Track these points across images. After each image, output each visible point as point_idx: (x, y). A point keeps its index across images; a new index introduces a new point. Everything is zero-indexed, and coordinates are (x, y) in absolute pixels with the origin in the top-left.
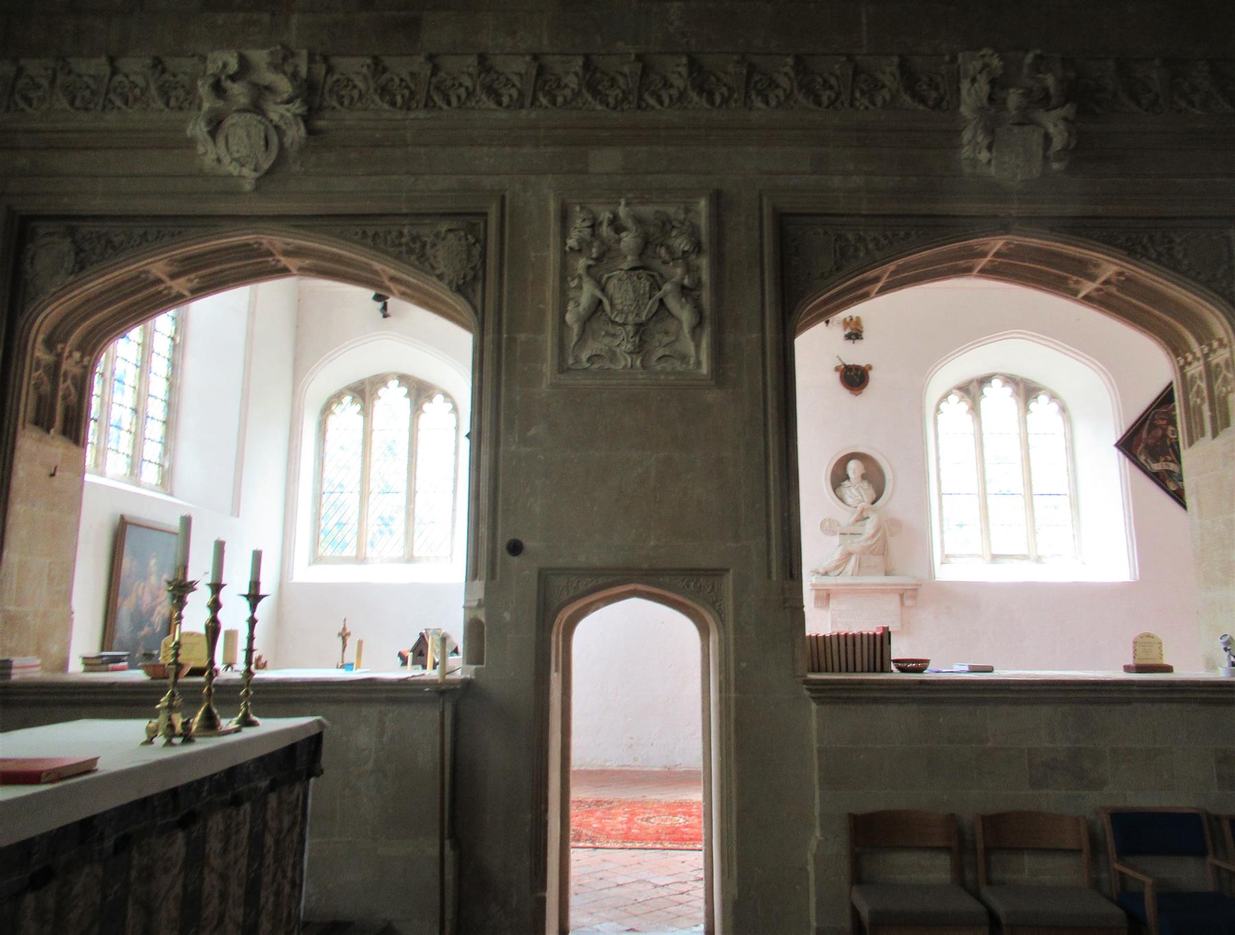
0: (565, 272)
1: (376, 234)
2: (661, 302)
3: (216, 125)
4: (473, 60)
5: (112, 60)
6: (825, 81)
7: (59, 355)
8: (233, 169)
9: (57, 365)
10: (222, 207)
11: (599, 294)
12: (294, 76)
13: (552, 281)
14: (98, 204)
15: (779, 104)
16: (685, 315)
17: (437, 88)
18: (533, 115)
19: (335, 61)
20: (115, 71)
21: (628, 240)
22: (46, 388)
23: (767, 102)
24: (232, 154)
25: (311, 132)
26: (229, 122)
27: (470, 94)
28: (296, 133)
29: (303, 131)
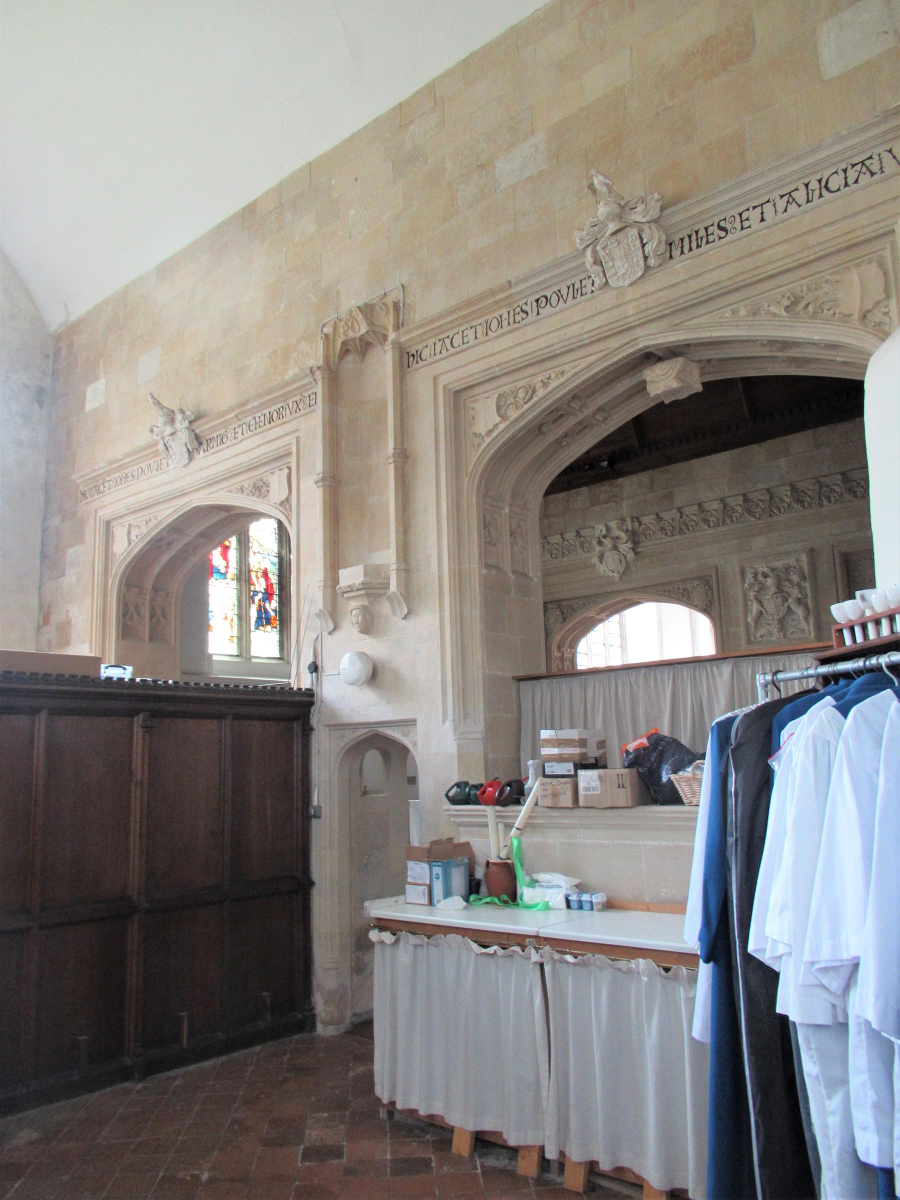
0: (746, 599)
1: (669, 591)
2: (789, 607)
3: (601, 558)
4: (695, 507)
5: (562, 535)
6: (858, 484)
7: (562, 652)
8: (610, 574)
9: (562, 657)
10: (608, 589)
11: (760, 608)
12: (627, 531)
13: (741, 602)
14: (567, 595)
15: (836, 501)
16: (799, 612)
17: (683, 524)
18: (724, 529)
19: (642, 519)
20: (564, 539)
21: (770, 581)
22: (560, 666)
23: (830, 501)
24: (609, 567)
25: (636, 553)
26: (605, 556)
27: (697, 524)
28: (631, 556)
29: (633, 555)
